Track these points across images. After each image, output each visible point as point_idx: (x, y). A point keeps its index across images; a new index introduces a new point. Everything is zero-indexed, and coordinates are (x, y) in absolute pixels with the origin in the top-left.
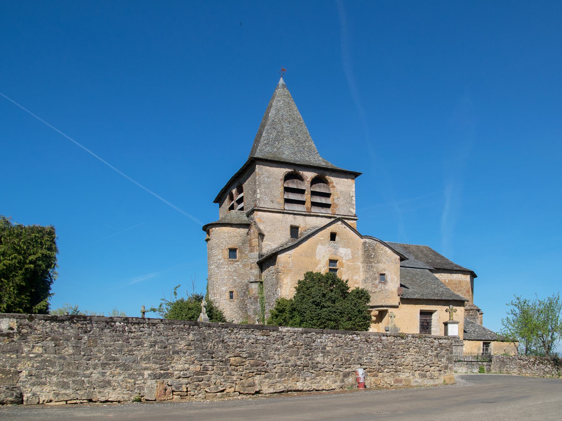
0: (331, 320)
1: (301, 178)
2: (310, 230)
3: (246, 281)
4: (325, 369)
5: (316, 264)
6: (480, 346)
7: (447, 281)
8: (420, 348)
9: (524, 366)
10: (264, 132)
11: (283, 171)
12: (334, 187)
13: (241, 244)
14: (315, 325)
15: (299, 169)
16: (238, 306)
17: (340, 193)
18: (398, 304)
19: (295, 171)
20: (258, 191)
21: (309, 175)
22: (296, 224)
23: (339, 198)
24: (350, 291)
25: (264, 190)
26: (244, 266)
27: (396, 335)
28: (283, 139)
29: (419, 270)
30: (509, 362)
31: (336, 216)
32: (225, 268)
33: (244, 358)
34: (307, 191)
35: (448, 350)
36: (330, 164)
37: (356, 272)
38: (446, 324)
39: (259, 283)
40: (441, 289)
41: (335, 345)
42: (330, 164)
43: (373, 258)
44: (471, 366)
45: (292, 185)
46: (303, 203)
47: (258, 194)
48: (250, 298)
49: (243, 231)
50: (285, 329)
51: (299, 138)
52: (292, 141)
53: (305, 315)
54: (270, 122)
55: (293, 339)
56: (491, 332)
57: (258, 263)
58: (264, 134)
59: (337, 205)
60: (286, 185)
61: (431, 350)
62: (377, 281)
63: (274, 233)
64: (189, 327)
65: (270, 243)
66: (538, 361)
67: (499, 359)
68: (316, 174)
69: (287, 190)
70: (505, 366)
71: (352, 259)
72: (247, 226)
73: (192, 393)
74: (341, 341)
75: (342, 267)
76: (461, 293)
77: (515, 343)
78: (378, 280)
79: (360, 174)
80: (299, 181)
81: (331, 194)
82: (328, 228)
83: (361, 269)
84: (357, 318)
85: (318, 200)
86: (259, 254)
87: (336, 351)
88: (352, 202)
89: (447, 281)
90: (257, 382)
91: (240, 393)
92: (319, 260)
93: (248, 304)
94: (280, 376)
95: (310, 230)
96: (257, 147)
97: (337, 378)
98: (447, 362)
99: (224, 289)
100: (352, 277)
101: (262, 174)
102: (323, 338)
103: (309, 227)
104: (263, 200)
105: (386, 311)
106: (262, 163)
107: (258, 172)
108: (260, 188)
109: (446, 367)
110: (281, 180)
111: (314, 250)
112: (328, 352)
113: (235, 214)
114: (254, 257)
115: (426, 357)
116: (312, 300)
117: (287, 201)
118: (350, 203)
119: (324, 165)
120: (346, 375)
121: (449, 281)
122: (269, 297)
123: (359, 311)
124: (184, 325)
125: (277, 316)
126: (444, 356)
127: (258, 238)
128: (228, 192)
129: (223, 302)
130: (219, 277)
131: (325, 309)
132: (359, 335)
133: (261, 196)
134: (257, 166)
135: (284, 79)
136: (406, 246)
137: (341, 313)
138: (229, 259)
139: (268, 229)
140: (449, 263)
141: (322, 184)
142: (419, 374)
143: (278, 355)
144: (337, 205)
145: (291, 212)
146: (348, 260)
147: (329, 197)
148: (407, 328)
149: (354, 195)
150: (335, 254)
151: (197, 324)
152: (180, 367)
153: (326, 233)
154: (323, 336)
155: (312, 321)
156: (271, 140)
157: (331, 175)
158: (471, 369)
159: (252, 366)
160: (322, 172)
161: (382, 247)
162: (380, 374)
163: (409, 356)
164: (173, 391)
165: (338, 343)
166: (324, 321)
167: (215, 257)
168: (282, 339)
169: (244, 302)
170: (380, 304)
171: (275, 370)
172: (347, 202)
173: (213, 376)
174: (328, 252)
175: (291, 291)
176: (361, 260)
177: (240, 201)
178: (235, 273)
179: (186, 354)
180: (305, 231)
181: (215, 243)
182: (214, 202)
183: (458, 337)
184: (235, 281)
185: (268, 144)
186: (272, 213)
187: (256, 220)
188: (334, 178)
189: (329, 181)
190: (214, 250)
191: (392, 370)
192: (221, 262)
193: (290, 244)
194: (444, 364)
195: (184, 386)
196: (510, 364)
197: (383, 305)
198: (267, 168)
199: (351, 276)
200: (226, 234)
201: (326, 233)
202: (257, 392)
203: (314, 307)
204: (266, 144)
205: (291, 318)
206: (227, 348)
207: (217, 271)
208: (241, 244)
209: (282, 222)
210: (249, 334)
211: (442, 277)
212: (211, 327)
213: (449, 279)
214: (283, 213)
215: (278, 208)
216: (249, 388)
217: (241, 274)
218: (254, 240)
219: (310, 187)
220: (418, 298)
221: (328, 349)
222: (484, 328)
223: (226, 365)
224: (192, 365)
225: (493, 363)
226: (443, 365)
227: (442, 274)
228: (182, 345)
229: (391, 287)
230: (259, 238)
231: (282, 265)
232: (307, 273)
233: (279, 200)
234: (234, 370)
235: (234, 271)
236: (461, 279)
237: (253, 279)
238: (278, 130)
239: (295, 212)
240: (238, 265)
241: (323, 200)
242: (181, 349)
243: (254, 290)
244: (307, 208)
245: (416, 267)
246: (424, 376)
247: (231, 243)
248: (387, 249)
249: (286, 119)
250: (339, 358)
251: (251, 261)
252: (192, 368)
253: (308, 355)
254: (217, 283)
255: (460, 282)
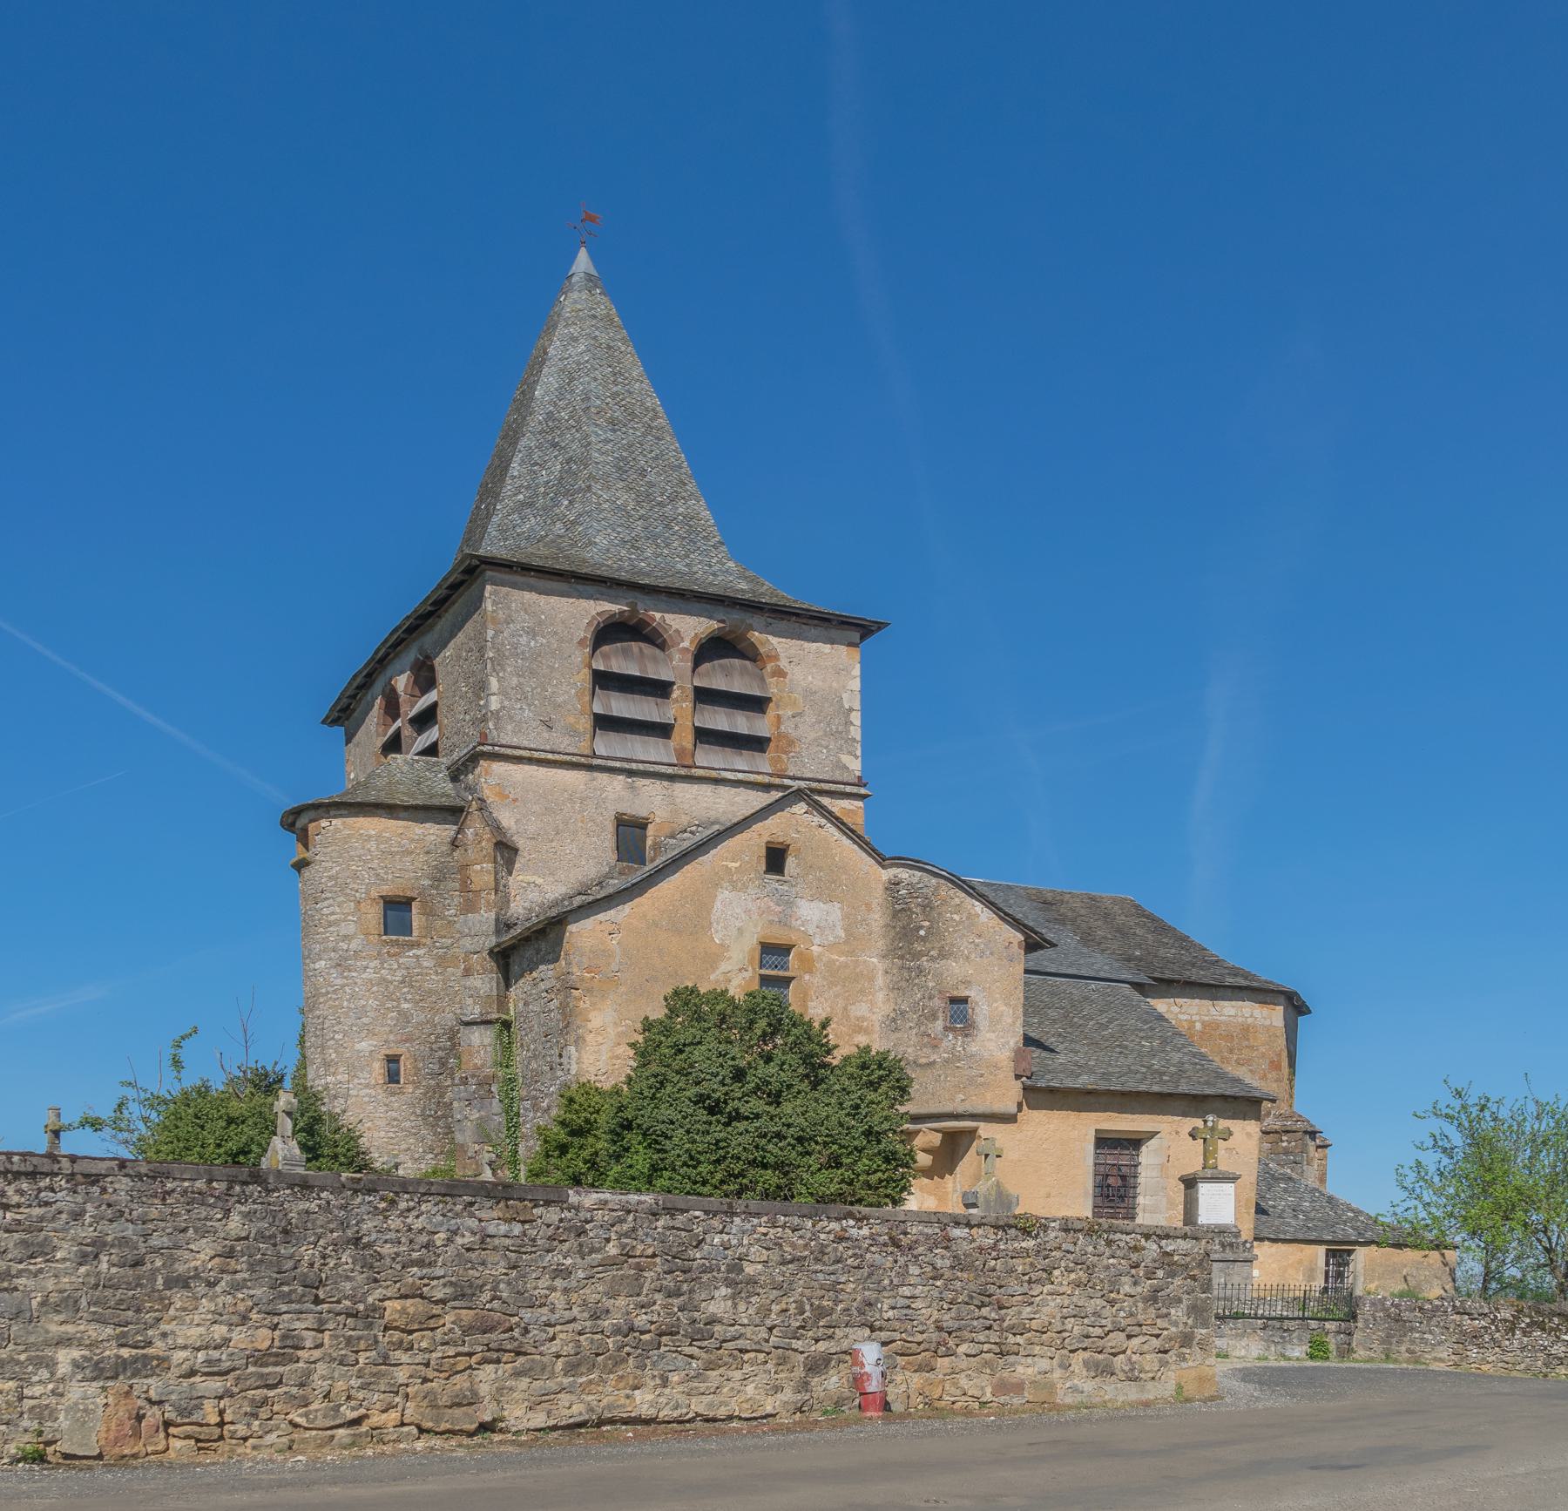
0: (765, 1166)
1: (655, 638)
2: (691, 832)
3: (448, 1019)
4: (741, 1343)
5: (713, 959)
6: (1316, 1264)
7: (1198, 1026)
8: (1090, 1270)
9: (1475, 1337)
10: (517, 459)
11: (591, 610)
12: (780, 673)
13: (427, 882)
14: (704, 1183)
15: (648, 602)
16: (418, 1112)
17: (805, 697)
18: (1013, 1109)
19: (634, 611)
20: (494, 683)
21: (688, 628)
22: (638, 809)
23: (800, 714)
24: (835, 1060)
25: (515, 681)
26: (442, 962)
27: (1001, 1223)
28: (589, 487)
29: (1093, 985)
30: (1421, 1323)
31: (787, 782)
32: (369, 971)
33: (437, 1303)
34: (680, 687)
35: (1194, 1278)
36: (765, 587)
37: (862, 991)
38: (1190, 1183)
39: (497, 1026)
40: (1176, 1057)
41: (775, 1256)
42: (765, 587)
43: (923, 939)
44: (1280, 1333)
45: (624, 660)
46: (662, 730)
47: (494, 694)
48: (464, 1081)
49: (435, 833)
50: (590, 1199)
51: (651, 485)
52: (624, 498)
53: (668, 1145)
54: (540, 423)
55: (620, 1236)
56: (1358, 1212)
57: (491, 952)
58: (515, 467)
59: (791, 743)
60: (600, 666)
61: (1133, 1276)
62: (939, 1024)
63: (554, 844)
64: (228, 1190)
65: (539, 881)
66: (1528, 1320)
67: (1385, 1310)
68: (715, 625)
69: (604, 681)
70: (1405, 1335)
71: (846, 942)
72: (453, 813)
73: (241, 1429)
74: (801, 1242)
75: (810, 972)
76: (1251, 1071)
77: (1443, 1255)
78: (941, 1019)
79: (880, 626)
80: (647, 649)
81: (769, 700)
82: (757, 827)
83: (880, 980)
84: (860, 1158)
85: (720, 719)
86: (497, 920)
87: (781, 1279)
88: (848, 732)
89: (1198, 1026)
90: (484, 1389)
91: (421, 1430)
92: (722, 945)
93: (456, 1104)
94: (572, 1369)
95: (691, 832)
96: (489, 516)
97: (782, 1375)
98: (1190, 1322)
99: (364, 1046)
100: (845, 1009)
101: (509, 621)
102: (734, 1231)
103: (684, 820)
104: (511, 718)
105: (972, 1133)
106: (507, 577)
107: (493, 611)
108: (501, 674)
109: (1186, 1340)
110: (581, 642)
111: (703, 907)
112: (752, 1281)
113: (405, 768)
114: (480, 930)
115: (1112, 1303)
116: (692, 1091)
117: (605, 723)
118: (841, 735)
119: (743, 590)
120: (818, 1365)
121: (1203, 1023)
122: (536, 1077)
123: (868, 1133)
124: (210, 1181)
125: (563, 1149)
126: (1180, 1301)
127: (495, 862)
128: (379, 686)
129: (362, 1093)
130: (345, 1004)
131: (741, 1126)
132: (865, 1222)
133: (506, 703)
134: (488, 588)
135: (593, 257)
136: (1049, 897)
137: (800, 1140)
138: (384, 937)
139: (532, 829)
140: (1206, 961)
141: (736, 662)
142: (1086, 1363)
143: (566, 1291)
144: (793, 742)
145: (618, 764)
146: (831, 947)
147: (764, 712)
148: (1048, 1196)
149: (857, 706)
150: (784, 923)
151: (257, 1177)
152: (194, 1334)
153: (754, 841)
154: (732, 1222)
155: (695, 1167)
156: (542, 490)
157: (770, 628)
158: (1279, 1347)
159: (466, 1331)
160: (736, 616)
161: (957, 901)
162: (943, 1363)
163: (1049, 1297)
164: (167, 1424)
165: (787, 1249)
166: (737, 1168)
167: (331, 929)
168: (581, 1233)
169: (442, 1096)
170: (948, 1108)
171: (554, 1347)
172: (831, 729)
173: (321, 1368)
174: (755, 917)
175: (618, 1057)
176: (881, 944)
177: (426, 719)
178: (405, 990)
179: (218, 1289)
180: (673, 837)
181: (330, 878)
182: (323, 722)
183: (1234, 1230)
184: (405, 1017)
185: (531, 505)
186: (546, 769)
187: (487, 793)
188: (781, 640)
189: (762, 650)
190: (326, 903)
191: (986, 1348)
192: (354, 945)
193: (615, 884)
194: (1177, 1326)
195: (209, 1405)
196: (1424, 1327)
197: (960, 1110)
198: (529, 596)
199: (841, 1003)
200: (372, 845)
201: (754, 841)
202: (485, 1427)
203: (702, 1115)
204: (523, 504)
205: (617, 1157)
206: (371, 1264)
207: (339, 981)
208: (427, 882)
209: (583, 800)
210: (457, 1215)
211: (1180, 1012)
212: (313, 1187)
213: (1206, 1018)
214: (590, 768)
215: (571, 750)
216: (458, 1412)
217: (430, 992)
218: (478, 867)
219: (689, 673)
220: (1090, 1087)
221: (749, 1269)
222: (1331, 1200)
223: (370, 1326)
224: (239, 1328)
225: (1360, 1324)
226: (1174, 1329)
227: (1180, 1001)
228: (202, 1253)
229: (991, 1046)
230: (499, 859)
231: (585, 960)
232: (676, 993)
233: (572, 720)
234: (399, 1345)
235: (403, 982)
236: (1250, 1021)
237: (474, 1011)
238: (571, 453)
239: (634, 766)
240: (420, 958)
241: (740, 723)
242: (196, 1269)
243: (478, 1052)
244: (680, 752)
245: (1083, 972)
246: (1103, 1370)
247: (390, 877)
248: (978, 907)
249: (598, 413)
250: (790, 1302)
251: (467, 943)
252: (239, 1337)
253: (678, 1294)
254: (339, 1023)
255: (1246, 1031)
